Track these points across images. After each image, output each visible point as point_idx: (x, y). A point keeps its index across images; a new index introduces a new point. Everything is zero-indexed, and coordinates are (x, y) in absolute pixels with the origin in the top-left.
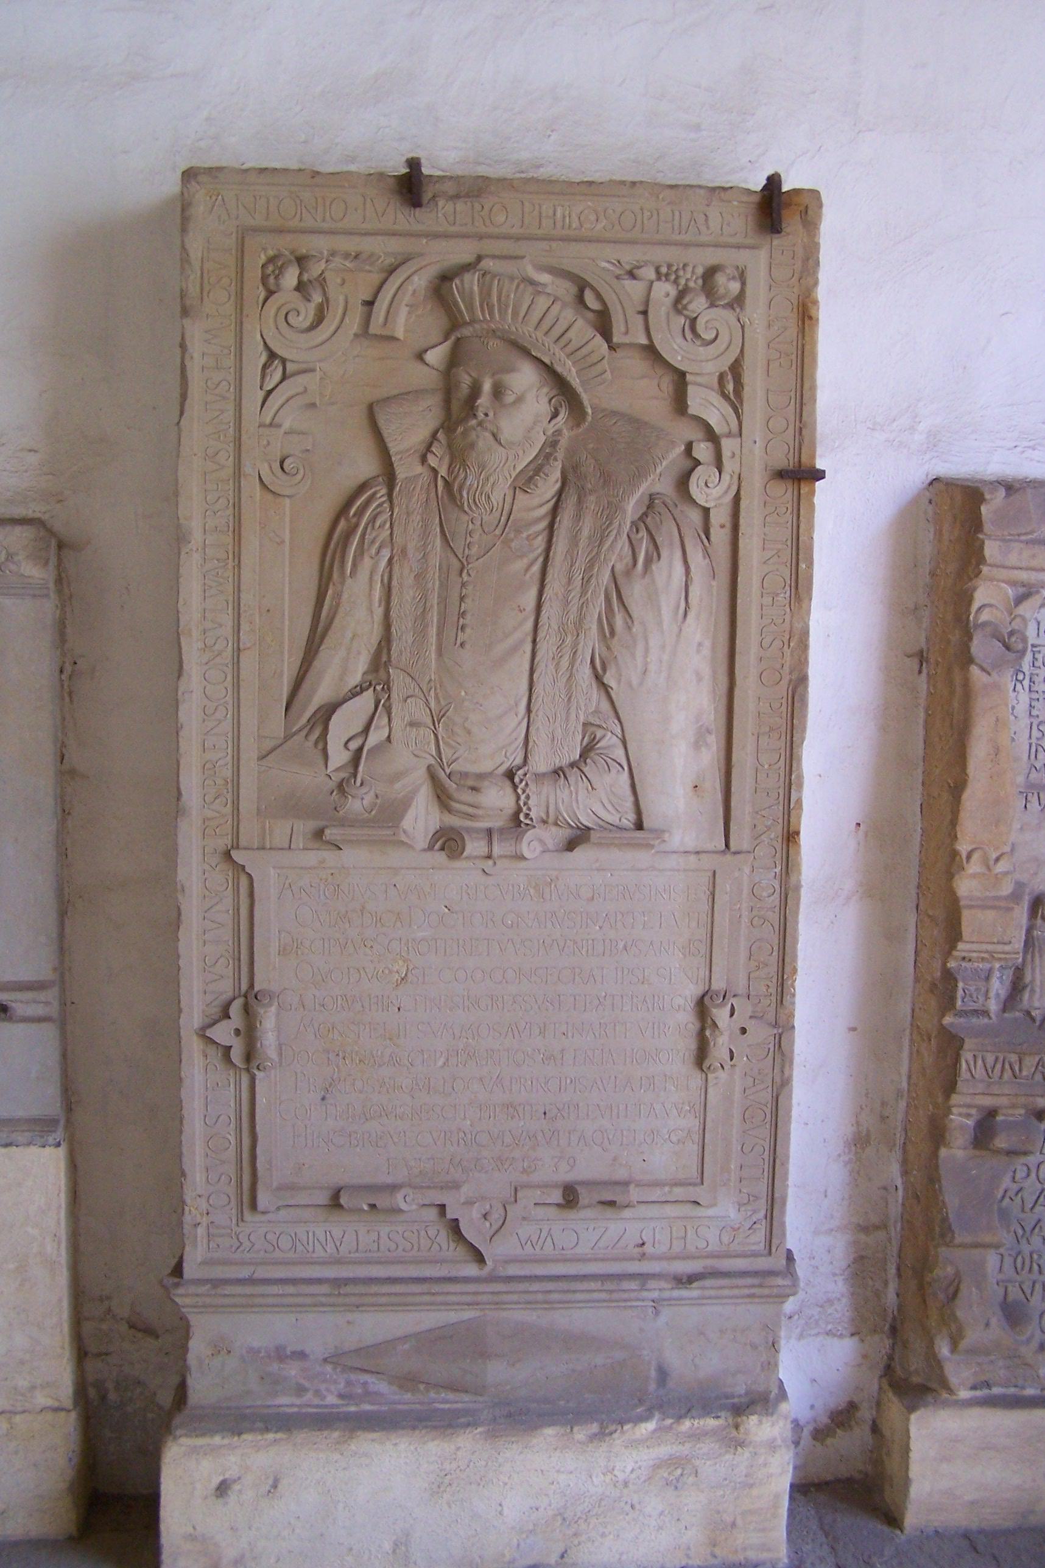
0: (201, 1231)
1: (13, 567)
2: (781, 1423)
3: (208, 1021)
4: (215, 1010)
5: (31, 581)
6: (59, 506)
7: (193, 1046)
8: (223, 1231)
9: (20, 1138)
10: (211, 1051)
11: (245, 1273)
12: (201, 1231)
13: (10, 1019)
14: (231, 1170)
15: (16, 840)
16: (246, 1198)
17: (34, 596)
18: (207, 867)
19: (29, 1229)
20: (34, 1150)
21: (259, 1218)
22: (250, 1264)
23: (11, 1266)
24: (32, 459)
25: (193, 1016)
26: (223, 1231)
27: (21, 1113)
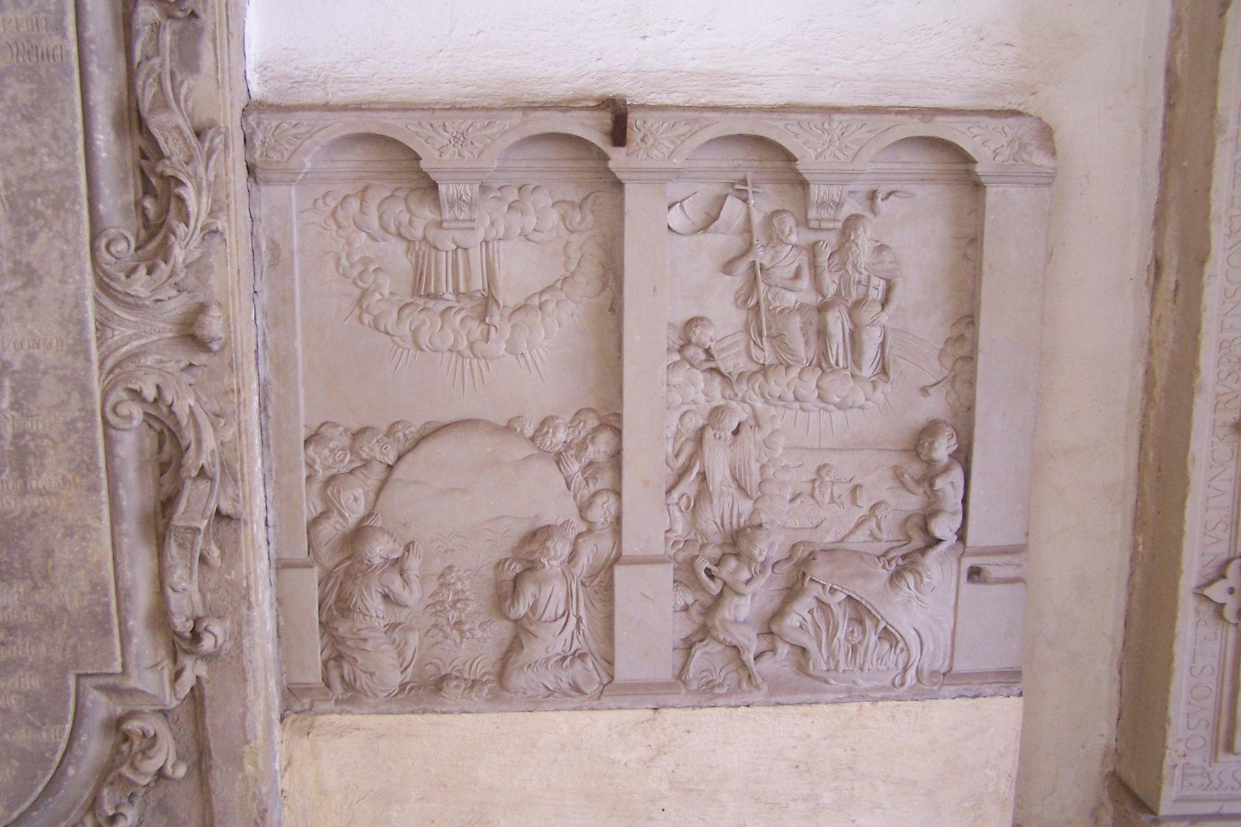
0: (1177, 772)
1: (1025, 156)
2: (377, 561)
3: (1204, 581)
4: (1211, 571)
5: (1040, 170)
6: (1032, 98)
7: (1187, 606)
8: (1195, 771)
9: (988, 689)
10: (1204, 607)
11: (1211, 808)
12: (1177, 772)
13: (985, 581)
14: (1209, 714)
15: (1004, 415)
16: (1222, 739)
17: (1037, 184)
18: (1216, 440)
19: (988, 771)
20: (1000, 700)
21: (1232, 758)
22: (1219, 800)
23: (967, 805)
24: (1008, 53)
25: (1188, 580)
26: (1195, 771)
27: (989, 667)
